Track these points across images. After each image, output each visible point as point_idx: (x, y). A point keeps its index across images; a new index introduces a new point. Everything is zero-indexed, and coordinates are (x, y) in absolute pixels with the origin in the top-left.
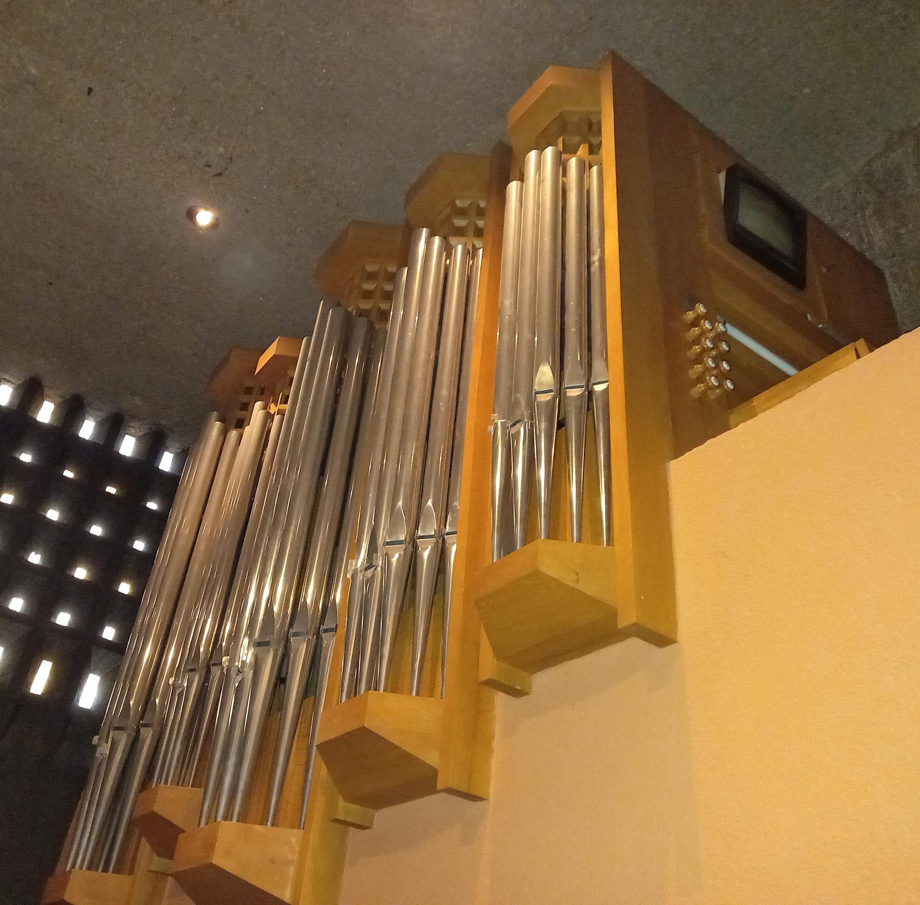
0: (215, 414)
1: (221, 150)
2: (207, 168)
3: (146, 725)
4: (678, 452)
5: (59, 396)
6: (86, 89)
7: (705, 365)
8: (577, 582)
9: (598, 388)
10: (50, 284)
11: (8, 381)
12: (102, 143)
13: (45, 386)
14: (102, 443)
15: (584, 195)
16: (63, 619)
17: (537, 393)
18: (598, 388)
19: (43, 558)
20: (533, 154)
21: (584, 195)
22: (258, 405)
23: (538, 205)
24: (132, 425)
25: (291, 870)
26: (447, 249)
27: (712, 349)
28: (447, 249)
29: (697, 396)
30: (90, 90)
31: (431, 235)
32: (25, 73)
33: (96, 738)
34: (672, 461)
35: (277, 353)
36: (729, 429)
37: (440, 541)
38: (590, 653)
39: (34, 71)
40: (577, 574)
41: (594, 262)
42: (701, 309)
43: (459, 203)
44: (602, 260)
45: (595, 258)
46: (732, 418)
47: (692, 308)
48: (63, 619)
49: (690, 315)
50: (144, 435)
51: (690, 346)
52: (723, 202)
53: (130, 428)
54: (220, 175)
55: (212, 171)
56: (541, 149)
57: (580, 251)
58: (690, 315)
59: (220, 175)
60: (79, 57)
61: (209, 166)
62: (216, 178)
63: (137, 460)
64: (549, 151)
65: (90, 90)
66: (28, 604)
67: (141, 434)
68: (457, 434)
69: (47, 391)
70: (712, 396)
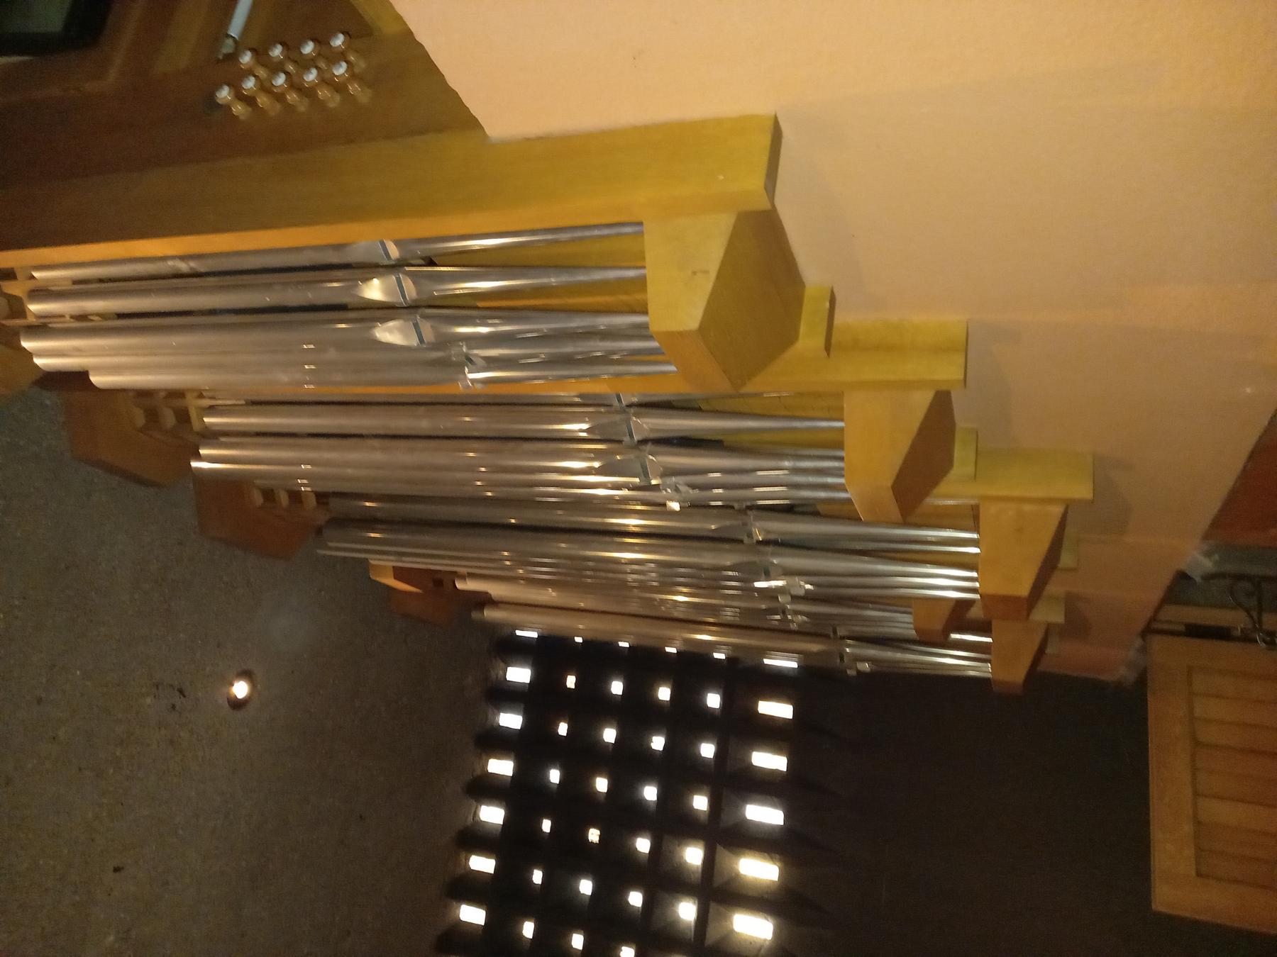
0: (475, 615)
1: (149, 700)
2: (177, 708)
3: (835, 632)
4: (471, 123)
5: (480, 758)
6: (117, 874)
7: (317, 85)
8: (706, 272)
9: (394, 252)
10: (361, 817)
11: (476, 808)
12: (181, 832)
13: (472, 775)
14: (522, 706)
15: (82, 288)
16: (713, 700)
17: (421, 340)
18: (394, 252)
19: (657, 734)
20: (38, 361)
21: (82, 288)
22: (460, 585)
23: (116, 352)
24: (495, 677)
25: (1027, 508)
26: (213, 436)
27: (287, 73)
28: (213, 436)
29: (368, 92)
30: (117, 870)
31: (199, 458)
32: (117, 946)
33: (849, 672)
34: (487, 133)
35: (392, 575)
36: (410, 33)
37: (632, 410)
38: (781, 221)
39: (111, 938)
40: (694, 273)
41: (191, 268)
42: (224, 94)
43: (140, 420)
44: (183, 258)
45: (183, 267)
46: (389, 28)
47: (227, 108)
48: (713, 700)
49: (239, 109)
50: (503, 661)
51: (289, 108)
52: (31, 58)
53: (499, 677)
54: (181, 692)
55: (178, 700)
56: (28, 355)
57: (175, 290)
58: (239, 109)
59: (181, 692)
60: (77, 898)
61: (173, 707)
62: (186, 694)
63: (533, 663)
64: (27, 344)
65: (117, 870)
66: (707, 739)
67: (502, 665)
68: (481, 400)
69: (478, 772)
70: (361, 65)
